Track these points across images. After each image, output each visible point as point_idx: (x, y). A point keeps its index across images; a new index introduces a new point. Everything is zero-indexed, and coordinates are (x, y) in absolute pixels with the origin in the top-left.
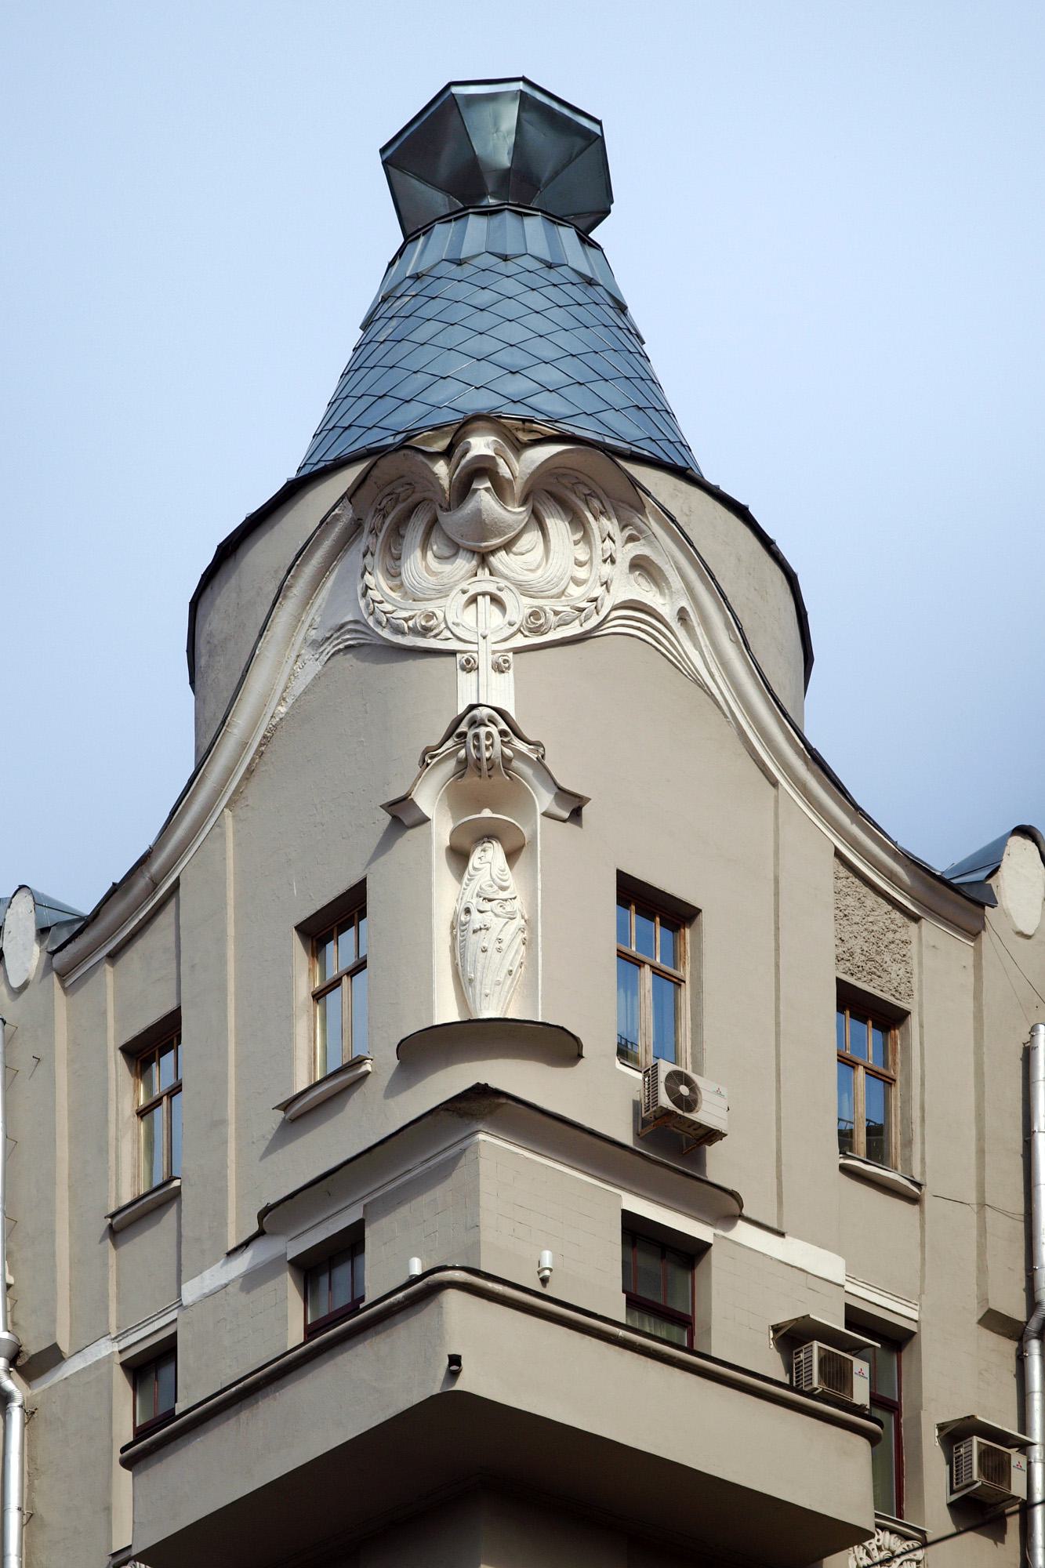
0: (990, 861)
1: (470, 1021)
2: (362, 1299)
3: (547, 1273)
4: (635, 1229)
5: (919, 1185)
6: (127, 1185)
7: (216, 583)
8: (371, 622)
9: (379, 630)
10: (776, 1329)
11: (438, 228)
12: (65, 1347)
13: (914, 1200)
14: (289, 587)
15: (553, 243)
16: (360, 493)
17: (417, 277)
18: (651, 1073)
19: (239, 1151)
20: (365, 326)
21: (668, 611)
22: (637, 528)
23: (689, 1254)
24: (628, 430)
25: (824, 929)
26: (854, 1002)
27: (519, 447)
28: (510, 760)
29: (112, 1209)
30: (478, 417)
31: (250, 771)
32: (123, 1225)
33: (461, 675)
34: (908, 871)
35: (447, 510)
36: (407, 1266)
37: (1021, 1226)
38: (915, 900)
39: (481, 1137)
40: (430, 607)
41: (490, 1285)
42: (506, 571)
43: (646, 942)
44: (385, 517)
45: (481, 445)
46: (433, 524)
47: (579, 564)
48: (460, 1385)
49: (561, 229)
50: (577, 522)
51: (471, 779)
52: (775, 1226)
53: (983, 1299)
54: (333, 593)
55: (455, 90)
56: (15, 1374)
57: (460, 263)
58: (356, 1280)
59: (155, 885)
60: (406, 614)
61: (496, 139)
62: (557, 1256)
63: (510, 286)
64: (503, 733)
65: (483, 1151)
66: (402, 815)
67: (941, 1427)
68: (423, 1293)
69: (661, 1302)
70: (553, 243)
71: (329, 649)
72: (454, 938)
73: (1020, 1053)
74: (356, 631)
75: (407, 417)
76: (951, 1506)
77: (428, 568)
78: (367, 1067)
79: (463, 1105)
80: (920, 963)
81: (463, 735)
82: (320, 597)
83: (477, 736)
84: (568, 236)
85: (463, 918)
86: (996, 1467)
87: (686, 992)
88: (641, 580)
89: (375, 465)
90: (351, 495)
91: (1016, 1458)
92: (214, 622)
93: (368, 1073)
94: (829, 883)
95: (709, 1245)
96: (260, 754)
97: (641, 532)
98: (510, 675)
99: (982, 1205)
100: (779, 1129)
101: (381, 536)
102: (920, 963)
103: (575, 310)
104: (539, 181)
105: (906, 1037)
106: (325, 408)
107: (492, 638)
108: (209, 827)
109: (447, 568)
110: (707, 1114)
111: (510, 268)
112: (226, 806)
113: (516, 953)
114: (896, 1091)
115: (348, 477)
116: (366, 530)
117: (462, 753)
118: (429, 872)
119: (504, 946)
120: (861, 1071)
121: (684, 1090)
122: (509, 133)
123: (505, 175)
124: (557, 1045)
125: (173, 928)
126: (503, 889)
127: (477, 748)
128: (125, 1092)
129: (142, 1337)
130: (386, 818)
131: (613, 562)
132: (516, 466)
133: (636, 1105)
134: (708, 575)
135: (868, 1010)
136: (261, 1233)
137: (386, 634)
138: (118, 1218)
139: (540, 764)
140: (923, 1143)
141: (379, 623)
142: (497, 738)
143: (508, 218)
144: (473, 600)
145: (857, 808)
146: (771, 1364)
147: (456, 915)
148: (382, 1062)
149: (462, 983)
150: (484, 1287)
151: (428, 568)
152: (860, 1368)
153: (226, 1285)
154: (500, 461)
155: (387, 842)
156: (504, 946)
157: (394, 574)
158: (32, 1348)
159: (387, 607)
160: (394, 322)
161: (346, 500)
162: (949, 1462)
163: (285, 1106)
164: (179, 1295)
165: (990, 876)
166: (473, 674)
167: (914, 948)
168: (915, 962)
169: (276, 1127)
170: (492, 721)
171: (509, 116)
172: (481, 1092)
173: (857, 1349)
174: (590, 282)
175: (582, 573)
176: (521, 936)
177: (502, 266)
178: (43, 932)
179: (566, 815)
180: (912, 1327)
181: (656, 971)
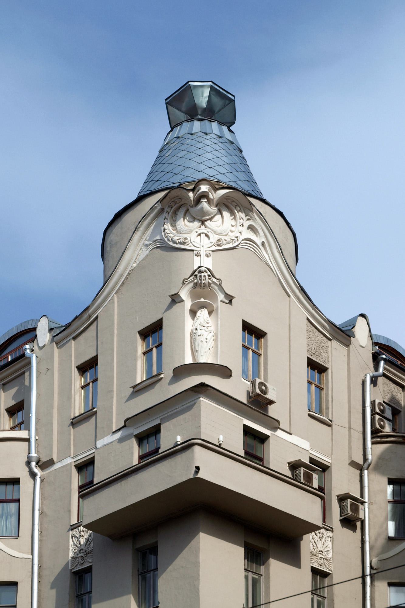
0: (352, 323)
2: (159, 448)
3: (221, 442)
4: (247, 431)
5: (331, 421)
6: (78, 409)
7: (113, 225)
8: (166, 239)
9: (168, 242)
10: (289, 463)
11: (184, 123)
12: (55, 460)
13: (330, 426)
14: (139, 228)
15: (221, 131)
16: (164, 200)
17: (178, 138)
18: (253, 383)
19: (117, 401)
20: (160, 152)
21: (259, 242)
22: (250, 216)
23: (263, 439)
24: (247, 188)
25: (304, 342)
26: (313, 365)
27: (216, 190)
28: (210, 284)
29: (73, 417)
30: (203, 180)
31: (123, 283)
32: (76, 422)
33: (195, 257)
34: (329, 325)
35: (192, 207)
36: (176, 439)
37: (362, 435)
38: (330, 334)
39: (201, 399)
40: (186, 236)
41: (209, 445)
42: (210, 227)
43: (250, 342)
45: (204, 188)
46: (187, 211)
47: (233, 226)
48: (199, 476)
49: (223, 127)
50: (232, 213)
51: (198, 289)
52: (288, 431)
53: (350, 457)
54: (153, 230)
55: (190, 83)
56: (38, 467)
57: (192, 134)
58: (158, 442)
59: (90, 317)
60: (178, 238)
61: (203, 98)
62: (224, 437)
63: (208, 142)
64: (209, 276)
65: (202, 403)
66: (175, 299)
67: (338, 496)
68: (187, 446)
69: (254, 453)
70: (221, 131)
71: (151, 247)
72: (191, 337)
73: (361, 382)
75: (176, 180)
76: (340, 520)
77: (185, 224)
78: (162, 376)
79: (196, 389)
80: (332, 353)
81: (196, 275)
82: (148, 232)
83: (201, 276)
84: (225, 128)
85: (195, 331)
86: (355, 509)
87: (262, 358)
88: (251, 232)
89: (169, 192)
90: (161, 201)
91: (361, 506)
92: (113, 236)
94: (305, 328)
95: (269, 436)
96: (127, 278)
97: (251, 217)
98: (210, 258)
99: (350, 428)
100: (290, 401)
101: (170, 214)
102: (332, 353)
103: (228, 150)
104: (214, 112)
105: (327, 376)
106: (147, 176)
107: (205, 247)
108: (109, 300)
109: (191, 224)
110: (270, 396)
111: (208, 137)
113: (211, 343)
114: (324, 392)
115: (161, 195)
116: (165, 211)
117: (196, 281)
118: (184, 317)
119: (208, 340)
120: (313, 385)
121: (264, 388)
122: (206, 97)
123: (204, 110)
124: (224, 372)
125: (96, 331)
126: (208, 323)
127: (201, 280)
128: (78, 381)
129: (82, 457)
130: (170, 300)
131: (243, 226)
132: (215, 195)
133: (248, 392)
134: (272, 232)
135: (316, 367)
136: (125, 426)
137: (171, 243)
138: (75, 420)
139: (220, 287)
140: (332, 408)
141: (169, 240)
142: (207, 277)
143: (206, 122)
144: (199, 235)
145: (314, 305)
146: (289, 473)
147: (192, 331)
148: (167, 374)
149: (194, 351)
150: (206, 445)
151: (185, 224)
152: (315, 476)
154: (210, 193)
155: (170, 307)
156: (208, 340)
157: (174, 225)
158: (44, 459)
159: (172, 235)
160: (171, 151)
161: (159, 202)
162: (340, 507)
163: (134, 387)
164: (96, 444)
165: (352, 328)
166: (199, 257)
167: (330, 348)
168: (330, 353)
169: (130, 393)
170: (206, 272)
171: (207, 92)
172: (202, 386)
173: (314, 470)
174: (232, 143)
175: (233, 229)
176: (213, 338)
177: (205, 136)
178: (51, 330)
179: (228, 302)
180: (329, 465)
181: (253, 351)
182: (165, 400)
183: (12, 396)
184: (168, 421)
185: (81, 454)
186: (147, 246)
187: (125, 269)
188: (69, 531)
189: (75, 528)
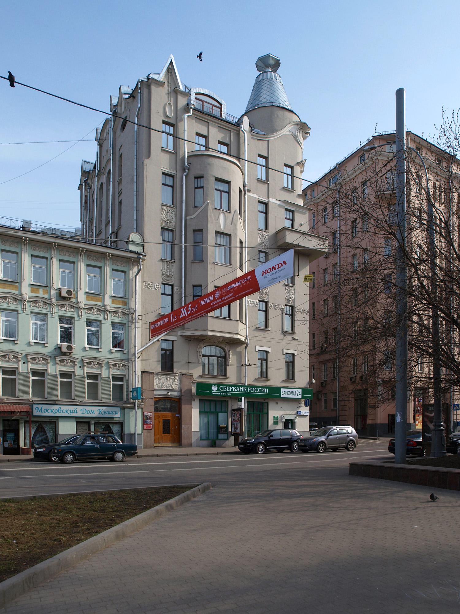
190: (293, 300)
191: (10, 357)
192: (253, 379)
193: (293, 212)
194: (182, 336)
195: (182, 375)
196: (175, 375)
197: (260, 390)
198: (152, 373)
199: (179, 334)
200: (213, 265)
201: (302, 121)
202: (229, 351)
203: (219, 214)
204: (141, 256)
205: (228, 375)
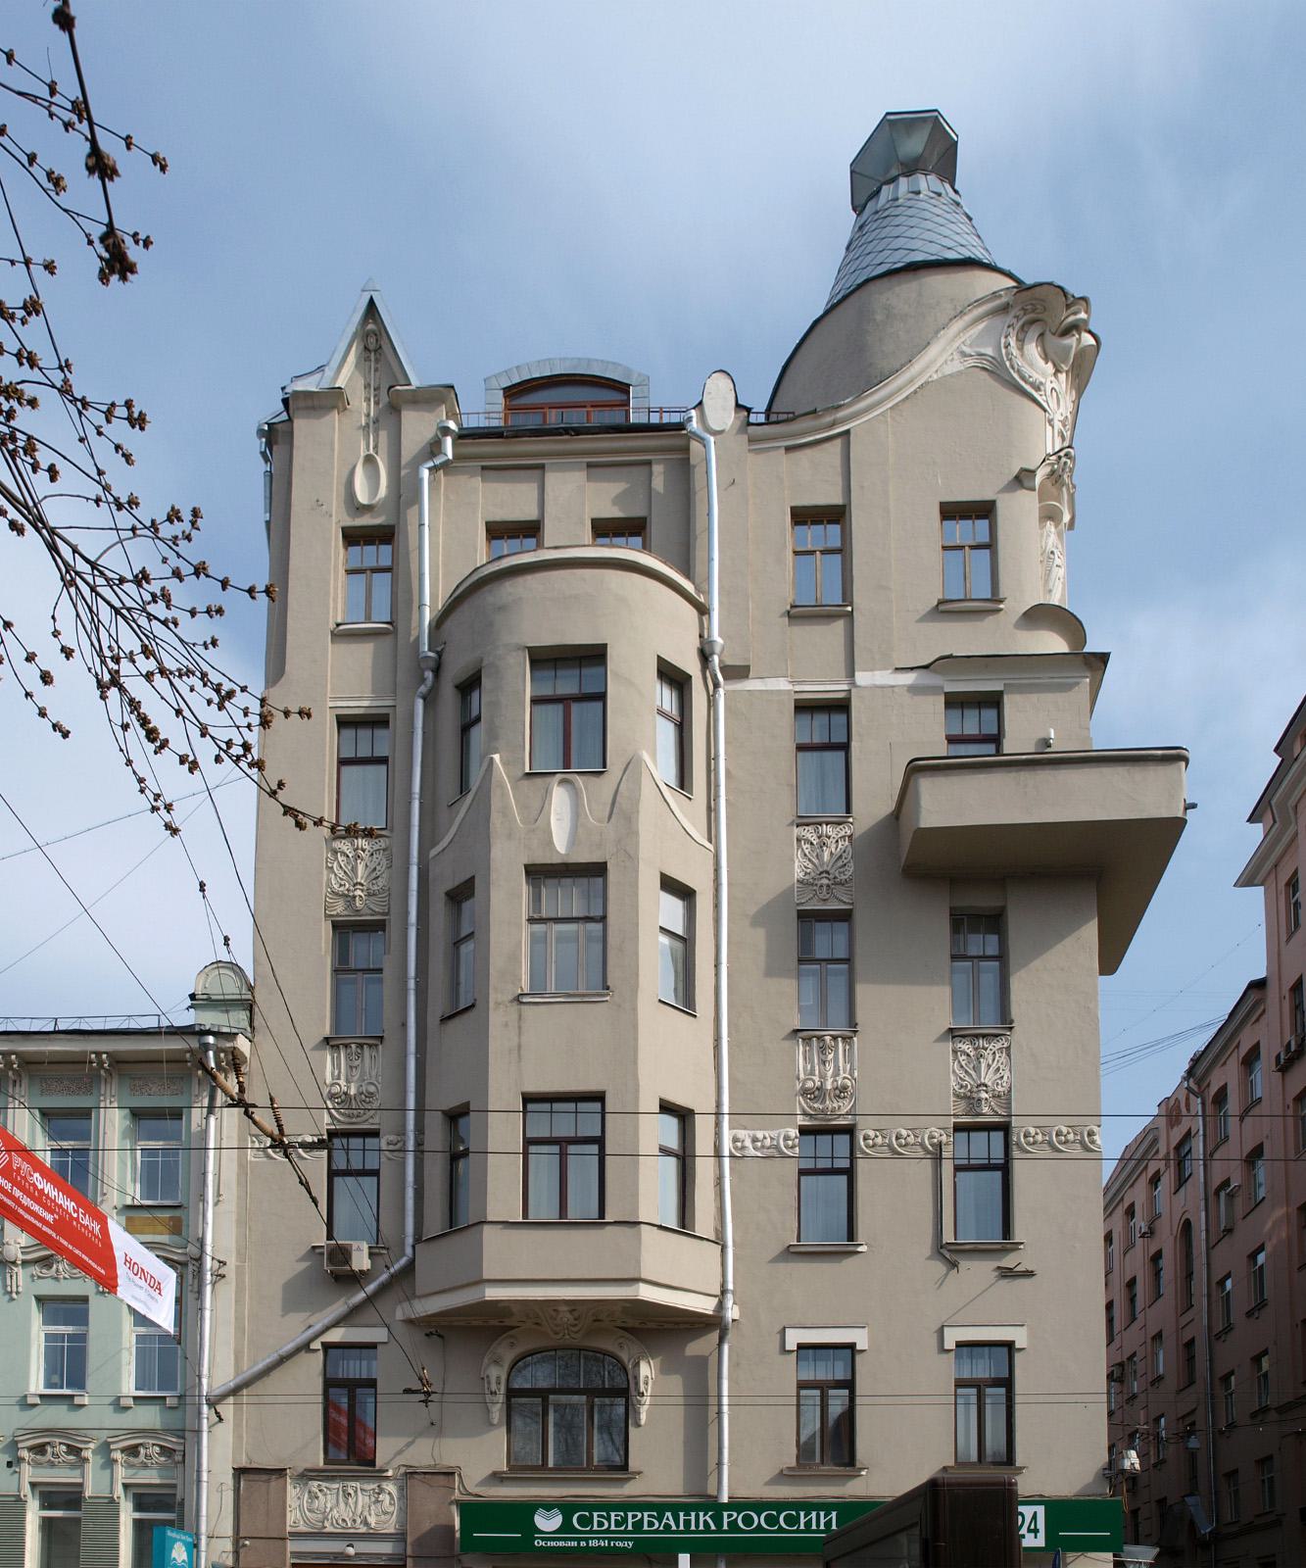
1: (1060, 607)
9: (1012, 371)
14: (965, 314)
31: (907, 398)
35: (1054, 334)
44: (1025, 314)
59: (833, 425)
74: (991, 362)
82: (972, 331)
93: (1001, 610)
96: (915, 392)
112: (891, 408)
153: (893, 687)
157: (1021, 342)
169: (928, 609)
182: (255, 804)
183: (613, 495)
184: (1021, 693)
185: (812, 682)
186: (964, 354)
187: (921, 373)
188: (792, 824)
189: (807, 825)
190: (1005, 1099)
191: (56, 1450)
192: (770, 1472)
193: (994, 701)
194: (410, 1322)
195: (410, 1474)
196: (379, 1476)
197: (792, 1520)
198: (280, 1472)
199: (399, 1315)
200: (515, 1006)
201: (1029, 281)
202: (637, 1365)
203: (547, 793)
204: (211, 1039)
205: (633, 1465)
